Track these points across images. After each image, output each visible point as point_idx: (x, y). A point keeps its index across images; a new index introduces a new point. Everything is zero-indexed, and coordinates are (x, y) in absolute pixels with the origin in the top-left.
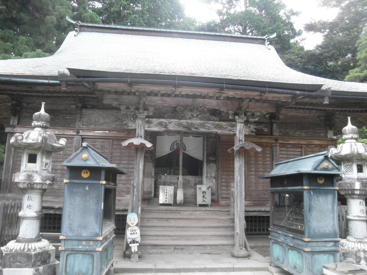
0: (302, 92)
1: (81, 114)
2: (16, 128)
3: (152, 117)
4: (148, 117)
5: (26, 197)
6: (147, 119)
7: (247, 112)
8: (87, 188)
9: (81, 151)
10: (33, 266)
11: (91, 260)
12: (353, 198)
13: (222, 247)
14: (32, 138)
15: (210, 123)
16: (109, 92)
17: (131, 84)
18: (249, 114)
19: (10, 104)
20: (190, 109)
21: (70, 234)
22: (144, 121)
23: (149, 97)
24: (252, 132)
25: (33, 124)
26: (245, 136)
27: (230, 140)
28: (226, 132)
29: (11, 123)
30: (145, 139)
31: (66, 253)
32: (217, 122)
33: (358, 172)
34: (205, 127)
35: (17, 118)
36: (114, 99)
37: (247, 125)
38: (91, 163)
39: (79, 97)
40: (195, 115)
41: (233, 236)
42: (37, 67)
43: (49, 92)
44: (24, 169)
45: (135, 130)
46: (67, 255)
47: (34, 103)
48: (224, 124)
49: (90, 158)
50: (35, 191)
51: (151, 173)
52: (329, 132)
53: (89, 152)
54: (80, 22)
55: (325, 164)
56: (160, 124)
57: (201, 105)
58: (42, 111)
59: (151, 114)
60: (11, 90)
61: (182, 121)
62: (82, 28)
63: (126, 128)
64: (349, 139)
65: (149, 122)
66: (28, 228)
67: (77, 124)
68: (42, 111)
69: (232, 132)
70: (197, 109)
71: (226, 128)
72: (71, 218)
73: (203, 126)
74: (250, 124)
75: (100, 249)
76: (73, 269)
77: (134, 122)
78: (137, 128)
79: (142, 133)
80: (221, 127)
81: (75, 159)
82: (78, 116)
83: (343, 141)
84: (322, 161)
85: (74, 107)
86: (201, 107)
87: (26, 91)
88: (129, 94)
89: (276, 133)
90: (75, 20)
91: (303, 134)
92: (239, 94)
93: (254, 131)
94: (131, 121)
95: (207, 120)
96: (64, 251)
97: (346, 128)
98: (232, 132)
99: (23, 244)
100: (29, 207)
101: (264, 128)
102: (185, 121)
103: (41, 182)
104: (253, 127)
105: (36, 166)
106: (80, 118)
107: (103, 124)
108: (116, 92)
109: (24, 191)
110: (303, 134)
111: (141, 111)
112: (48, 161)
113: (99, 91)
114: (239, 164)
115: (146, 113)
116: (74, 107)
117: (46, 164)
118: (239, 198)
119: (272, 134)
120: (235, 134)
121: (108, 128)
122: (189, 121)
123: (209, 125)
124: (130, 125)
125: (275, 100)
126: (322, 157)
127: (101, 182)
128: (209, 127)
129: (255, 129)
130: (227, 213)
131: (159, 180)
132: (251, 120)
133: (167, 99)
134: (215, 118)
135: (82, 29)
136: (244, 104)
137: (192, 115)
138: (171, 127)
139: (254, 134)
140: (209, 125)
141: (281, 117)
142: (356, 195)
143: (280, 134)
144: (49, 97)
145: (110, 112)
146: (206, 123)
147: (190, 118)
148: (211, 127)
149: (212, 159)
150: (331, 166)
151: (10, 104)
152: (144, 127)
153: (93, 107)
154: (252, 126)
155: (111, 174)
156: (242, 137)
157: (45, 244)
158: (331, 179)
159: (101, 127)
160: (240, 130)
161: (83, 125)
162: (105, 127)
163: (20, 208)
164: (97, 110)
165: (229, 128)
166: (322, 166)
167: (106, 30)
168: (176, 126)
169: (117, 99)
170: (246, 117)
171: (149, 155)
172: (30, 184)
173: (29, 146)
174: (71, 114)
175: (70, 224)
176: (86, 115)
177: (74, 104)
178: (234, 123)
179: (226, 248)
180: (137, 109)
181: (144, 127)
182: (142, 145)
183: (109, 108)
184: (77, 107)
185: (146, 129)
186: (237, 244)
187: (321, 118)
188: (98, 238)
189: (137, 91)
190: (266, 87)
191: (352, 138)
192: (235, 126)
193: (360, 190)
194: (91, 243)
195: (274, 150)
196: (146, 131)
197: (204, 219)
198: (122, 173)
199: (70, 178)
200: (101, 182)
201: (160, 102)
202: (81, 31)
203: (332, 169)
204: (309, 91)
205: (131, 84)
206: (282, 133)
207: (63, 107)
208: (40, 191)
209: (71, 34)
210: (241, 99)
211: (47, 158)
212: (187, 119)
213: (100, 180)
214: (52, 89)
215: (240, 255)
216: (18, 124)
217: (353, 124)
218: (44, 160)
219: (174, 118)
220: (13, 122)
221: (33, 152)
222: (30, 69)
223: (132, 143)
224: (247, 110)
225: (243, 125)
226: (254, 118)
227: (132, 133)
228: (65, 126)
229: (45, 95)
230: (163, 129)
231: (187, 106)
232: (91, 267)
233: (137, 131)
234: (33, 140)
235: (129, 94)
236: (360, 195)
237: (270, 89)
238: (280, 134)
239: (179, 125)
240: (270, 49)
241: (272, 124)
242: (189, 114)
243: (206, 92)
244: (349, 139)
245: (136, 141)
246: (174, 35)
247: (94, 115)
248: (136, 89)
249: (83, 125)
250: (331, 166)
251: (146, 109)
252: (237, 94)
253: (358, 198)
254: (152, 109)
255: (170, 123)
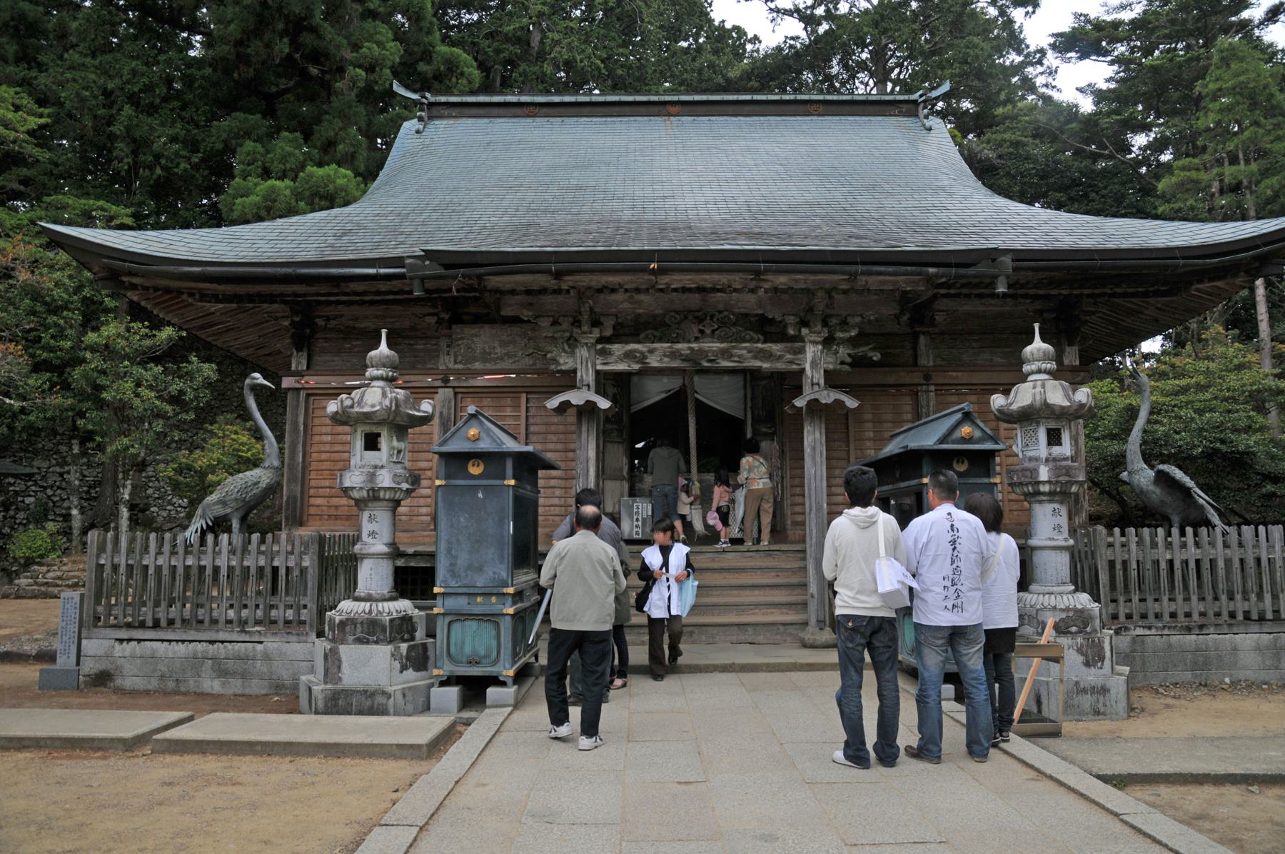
0: (942, 270)
1: (450, 336)
2: (306, 378)
3: (608, 340)
4: (601, 340)
5: (366, 515)
6: (599, 346)
7: (831, 316)
8: (480, 495)
9: (466, 423)
10: (390, 642)
11: (494, 632)
12: (1041, 502)
13: (782, 629)
14: (369, 402)
15: (745, 348)
16: (513, 292)
17: (558, 275)
18: (834, 321)
19: (286, 323)
20: (696, 318)
21: (453, 584)
22: (593, 351)
23: (602, 296)
24: (842, 363)
25: (367, 374)
26: (827, 373)
27: (792, 382)
28: (780, 366)
29: (293, 368)
30: (598, 392)
31: (448, 619)
32: (760, 345)
33: (1061, 445)
34: (732, 356)
35: (305, 354)
36: (523, 305)
37: (830, 349)
38: (485, 445)
39: (452, 301)
40: (708, 332)
41: (805, 605)
42: (344, 234)
43: (378, 293)
44: (359, 463)
45: (575, 371)
46: (450, 624)
47: (342, 316)
48: (776, 348)
49: (483, 435)
50: (380, 504)
51: (621, 469)
52: (1068, 349)
53: (481, 423)
54: (428, 95)
55: (966, 430)
56: (629, 356)
57: (721, 307)
58: (383, 348)
59: (608, 333)
60: (296, 295)
61: (679, 346)
62: (435, 111)
63: (553, 367)
64: (1033, 373)
65: (604, 353)
66: (374, 576)
67: (441, 361)
68: (383, 348)
69: (794, 367)
70: (712, 317)
71: (780, 357)
72: (453, 552)
73: (726, 354)
74: (838, 345)
75: (511, 611)
76: (462, 649)
77: (572, 353)
78: (579, 366)
79: (590, 378)
80: (769, 356)
81: (454, 438)
82: (443, 343)
83: (1024, 378)
84: (958, 425)
85: (432, 320)
86: (720, 312)
87: (324, 295)
88: (558, 292)
89: (927, 360)
90: (415, 91)
91: (999, 360)
92: (801, 280)
93: (848, 360)
94: (564, 351)
95: (736, 341)
96: (443, 614)
97: (1028, 349)
98: (794, 367)
99: (368, 604)
100: (372, 534)
101: (870, 354)
102: (686, 345)
103: (393, 485)
104: (843, 352)
105: (382, 456)
106: (448, 346)
107: (502, 359)
108: (529, 292)
109: (361, 504)
110: (999, 360)
111: (585, 328)
112: (402, 445)
113: (490, 291)
114: (813, 438)
115: (596, 333)
116: (432, 320)
117: (399, 452)
118: (813, 515)
119: (915, 364)
120: (804, 370)
121: (514, 367)
122: (695, 345)
123: (740, 352)
124: (562, 361)
125: (886, 288)
126: (959, 415)
127: (506, 482)
128: (740, 356)
129: (849, 355)
130: (800, 555)
131: (638, 486)
132: (840, 335)
133: (643, 297)
134: (755, 336)
135: (435, 111)
136: (820, 302)
137: (702, 332)
138: (654, 362)
139: (847, 367)
140: (740, 352)
141: (939, 318)
142: (1044, 494)
143: (939, 362)
144: (377, 302)
145: (516, 329)
146: (734, 347)
147: (697, 339)
148: (749, 354)
149: (764, 430)
150: (977, 434)
151: (286, 323)
152: (594, 365)
153: (478, 320)
154: (841, 350)
155: (528, 466)
156: (819, 377)
157: (404, 606)
158: (982, 461)
159: (498, 367)
160: (813, 360)
161: (456, 362)
162: (506, 365)
163: (357, 539)
164: (487, 327)
165: (789, 356)
166: (957, 435)
167: (495, 111)
168: (666, 359)
169: (531, 304)
170: (826, 330)
171: (615, 426)
172: (373, 489)
173: (367, 417)
174: (426, 338)
175: (451, 565)
176: (463, 339)
177: (433, 315)
178: (797, 345)
179: (791, 630)
180: (577, 323)
181: (594, 365)
182: (590, 408)
183: (515, 320)
184: (439, 322)
185: (599, 367)
186: (813, 621)
187: (1045, 315)
188: (505, 590)
189: (573, 287)
190: (856, 263)
191: (1039, 371)
192: (802, 351)
193: (1049, 482)
194: (494, 599)
195: (923, 401)
196: (598, 373)
197: (743, 570)
198: (549, 466)
199: (447, 477)
200: (506, 482)
201: (625, 305)
202: (431, 118)
203: (979, 441)
204: (958, 265)
205: (558, 275)
206: (944, 359)
207: (407, 324)
208: (391, 504)
209: (409, 126)
210: (808, 292)
211: (398, 440)
212: (689, 342)
213: (504, 478)
214: (383, 287)
215: (818, 643)
216: (308, 367)
217: (1044, 340)
218: (395, 443)
219: (661, 340)
220: (299, 363)
221: (375, 430)
222: (331, 240)
223: (568, 402)
224: (828, 312)
225: (820, 347)
226: (846, 331)
227: (569, 380)
228: (414, 368)
229: (367, 298)
230: (636, 367)
231: (689, 311)
232: (494, 643)
233: (579, 374)
234: (373, 406)
235: (558, 292)
236: (1051, 494)
237: (865, 268)
238: (939, 362)
239: (674, 355)
240: (930, 129)
241: (915, 337)
242: (695, 329)
243: (725, 281)
244: (1033, 373)
245: (576, 398)
246: (673, 109)
247: (483, 338)
248: (571, 284)
249: (456, 362)
250: (977, 434)
251: (596, 323)
252: (796, 281)
253: (1050, 501)
254: (609, 324)
255: (651, 351)
